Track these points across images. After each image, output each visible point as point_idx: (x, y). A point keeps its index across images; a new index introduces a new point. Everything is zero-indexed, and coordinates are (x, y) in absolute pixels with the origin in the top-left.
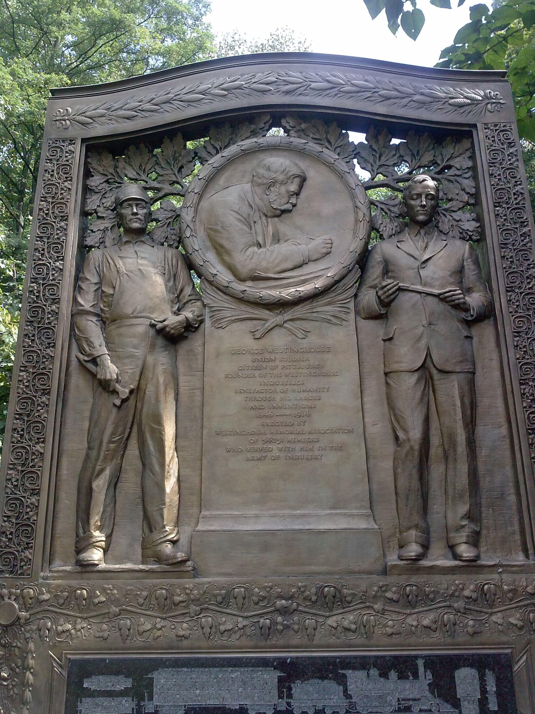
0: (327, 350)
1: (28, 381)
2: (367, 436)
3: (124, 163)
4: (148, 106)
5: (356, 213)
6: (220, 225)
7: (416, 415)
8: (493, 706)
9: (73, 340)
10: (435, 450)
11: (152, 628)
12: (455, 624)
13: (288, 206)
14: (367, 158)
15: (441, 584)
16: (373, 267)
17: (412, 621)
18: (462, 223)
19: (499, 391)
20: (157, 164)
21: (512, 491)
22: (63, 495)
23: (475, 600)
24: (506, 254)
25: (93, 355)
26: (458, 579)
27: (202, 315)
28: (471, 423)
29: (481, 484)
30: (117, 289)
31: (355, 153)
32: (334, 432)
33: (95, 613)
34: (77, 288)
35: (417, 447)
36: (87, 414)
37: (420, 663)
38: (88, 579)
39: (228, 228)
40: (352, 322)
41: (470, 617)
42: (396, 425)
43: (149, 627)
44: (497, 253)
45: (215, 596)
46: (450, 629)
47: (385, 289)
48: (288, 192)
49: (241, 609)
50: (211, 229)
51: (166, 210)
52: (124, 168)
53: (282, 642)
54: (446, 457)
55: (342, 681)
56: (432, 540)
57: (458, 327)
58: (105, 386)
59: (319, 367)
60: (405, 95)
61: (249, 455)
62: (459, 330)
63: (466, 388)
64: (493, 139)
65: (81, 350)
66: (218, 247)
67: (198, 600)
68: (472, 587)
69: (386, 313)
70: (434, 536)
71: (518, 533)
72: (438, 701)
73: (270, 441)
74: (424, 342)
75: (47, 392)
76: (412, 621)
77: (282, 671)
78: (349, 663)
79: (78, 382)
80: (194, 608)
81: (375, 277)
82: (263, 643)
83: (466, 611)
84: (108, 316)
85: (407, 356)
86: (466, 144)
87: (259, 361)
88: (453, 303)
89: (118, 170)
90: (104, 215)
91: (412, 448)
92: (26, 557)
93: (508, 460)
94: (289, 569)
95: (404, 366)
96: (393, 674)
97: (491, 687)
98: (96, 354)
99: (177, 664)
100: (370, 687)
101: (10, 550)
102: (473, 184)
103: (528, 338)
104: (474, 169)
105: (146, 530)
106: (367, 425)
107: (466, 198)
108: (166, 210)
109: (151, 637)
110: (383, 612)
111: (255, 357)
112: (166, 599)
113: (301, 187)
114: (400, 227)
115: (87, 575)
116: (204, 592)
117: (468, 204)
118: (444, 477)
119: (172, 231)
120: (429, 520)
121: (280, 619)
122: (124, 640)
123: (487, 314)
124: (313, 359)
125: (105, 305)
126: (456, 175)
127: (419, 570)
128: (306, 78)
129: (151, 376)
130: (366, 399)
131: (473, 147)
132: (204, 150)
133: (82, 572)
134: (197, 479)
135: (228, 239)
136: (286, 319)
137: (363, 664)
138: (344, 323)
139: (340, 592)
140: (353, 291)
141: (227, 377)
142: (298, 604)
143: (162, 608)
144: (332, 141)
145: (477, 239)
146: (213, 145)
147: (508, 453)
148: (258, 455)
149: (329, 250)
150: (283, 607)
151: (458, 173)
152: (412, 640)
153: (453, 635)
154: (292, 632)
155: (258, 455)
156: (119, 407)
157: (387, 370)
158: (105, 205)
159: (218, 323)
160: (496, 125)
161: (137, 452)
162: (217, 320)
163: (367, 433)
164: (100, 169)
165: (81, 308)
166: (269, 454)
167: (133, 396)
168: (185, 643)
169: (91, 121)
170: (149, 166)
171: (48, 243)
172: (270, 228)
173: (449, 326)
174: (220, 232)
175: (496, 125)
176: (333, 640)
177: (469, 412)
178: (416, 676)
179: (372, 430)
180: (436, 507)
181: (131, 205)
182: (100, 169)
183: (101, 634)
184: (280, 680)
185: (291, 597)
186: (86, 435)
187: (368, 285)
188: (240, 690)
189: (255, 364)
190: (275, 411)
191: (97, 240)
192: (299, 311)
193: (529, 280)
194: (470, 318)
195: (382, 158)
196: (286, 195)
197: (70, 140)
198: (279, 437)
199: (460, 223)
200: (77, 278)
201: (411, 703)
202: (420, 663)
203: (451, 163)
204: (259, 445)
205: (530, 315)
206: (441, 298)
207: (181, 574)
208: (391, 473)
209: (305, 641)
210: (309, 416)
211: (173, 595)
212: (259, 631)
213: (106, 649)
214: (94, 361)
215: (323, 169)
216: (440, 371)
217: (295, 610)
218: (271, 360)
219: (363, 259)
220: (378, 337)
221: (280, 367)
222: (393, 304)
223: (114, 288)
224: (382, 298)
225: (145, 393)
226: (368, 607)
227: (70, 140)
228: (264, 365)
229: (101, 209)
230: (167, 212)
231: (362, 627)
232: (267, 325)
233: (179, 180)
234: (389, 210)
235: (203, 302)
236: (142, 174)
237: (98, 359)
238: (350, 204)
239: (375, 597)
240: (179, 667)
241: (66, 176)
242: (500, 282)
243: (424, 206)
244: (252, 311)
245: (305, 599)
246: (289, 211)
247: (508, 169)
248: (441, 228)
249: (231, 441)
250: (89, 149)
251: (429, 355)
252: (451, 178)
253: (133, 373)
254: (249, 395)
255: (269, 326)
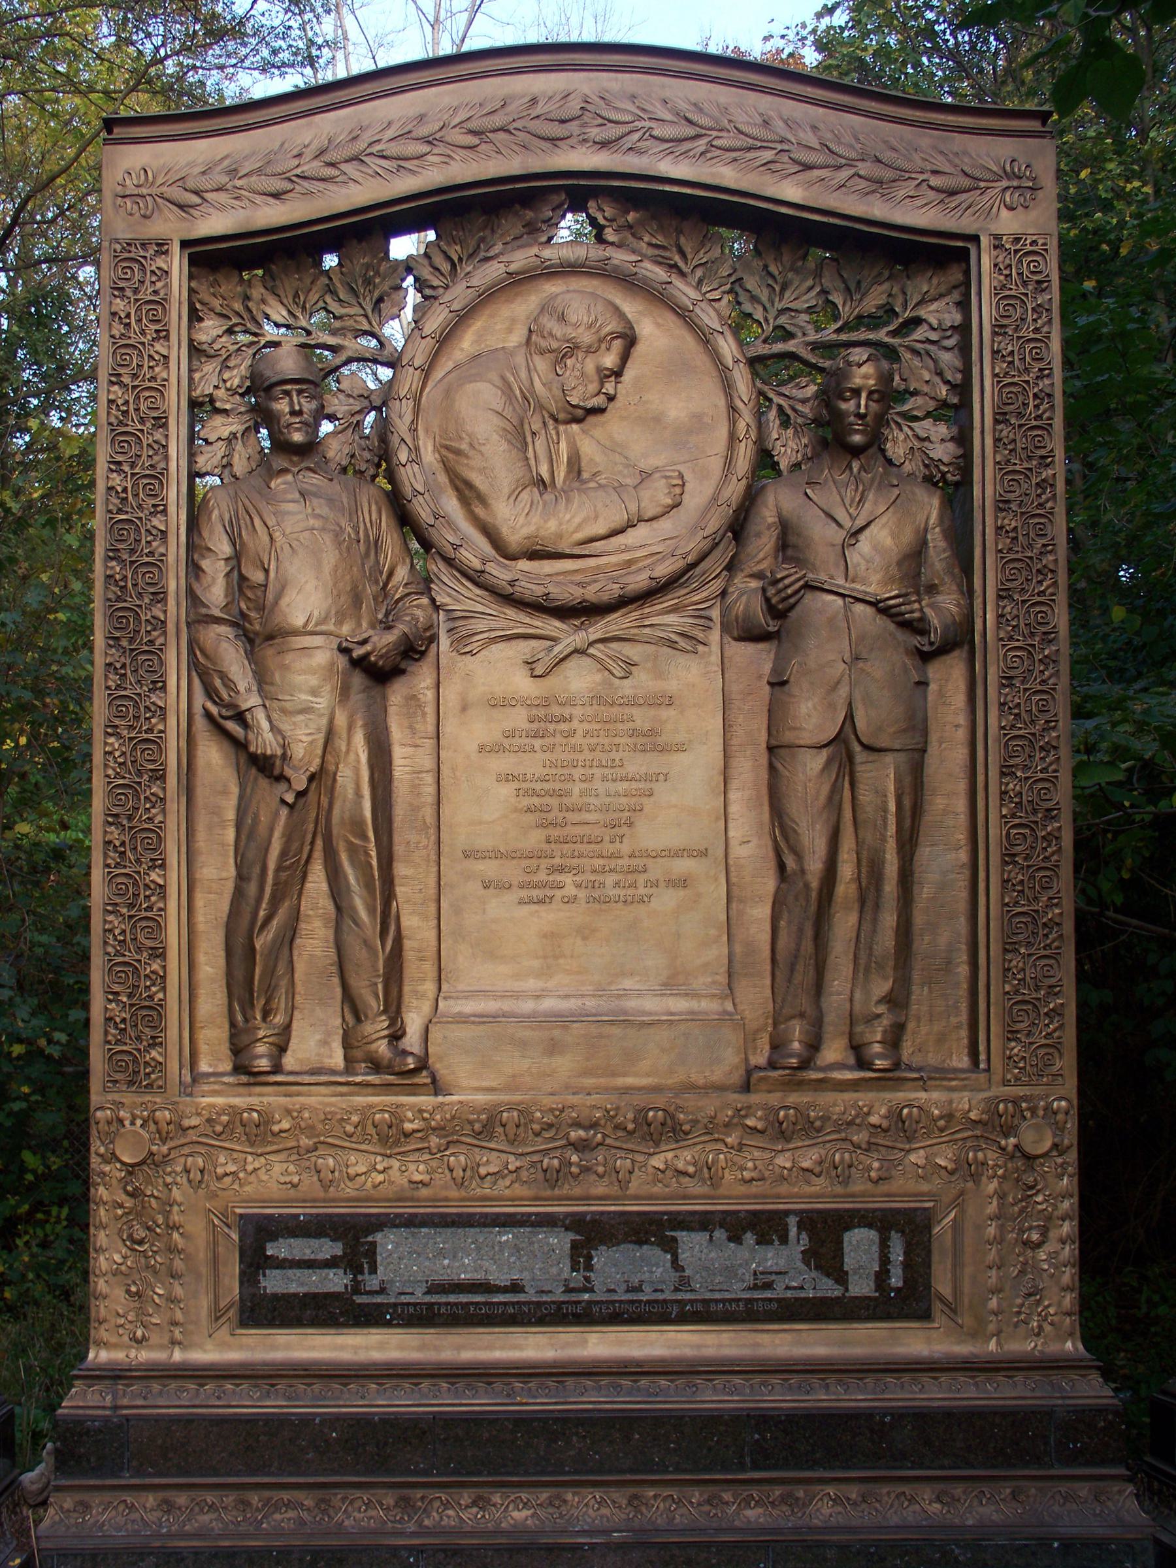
0: (669, 701)
1: (124, 753)
2: (731, 862)
3: (263, 290)
4: (311, 167)
5: (732, 423)
6: (467, 440)
7: (818, 827)
8: (896, 1281)
9: (194, 673)
10: (845, 888)
11: (371, 1177)
12: (850, 1166)
13: (599, 401)
14: (756, 291)
15: (835, 1105)
16: (758, 535)
17: (784, 1161)
18: (931, 446)
19: (962, 786)
20: (332, 292)
21: (965, 958)
22: (201, 958)
23: (886, 1131)
24: (1006, 521)
25: (237, 706)
26: (863, 1098)
27: (431, 626)
28: (908, 843)
29: (915, 946)
30: (272, 574)
31: (732, 279)
32: (678, 853)
33: (275, 1147)
34: (194, 569)
35: (815, 885)
36: (231, 815)
37: (792, 1221)
38: (260, 1095)
39: (483, 449)
40: (715, 648)
41: (875, 1155)
42: (782, 844)
43: (362, 1169)
44: (989, 521)
45: (471, 1122)
46: (841, 1174)
47: (781, 585)
48: (599, 369)
49: (512, 1142)
50: (447, 448)
51: (349, 396)
52: (263, 301)
53: (577, 1191)
54: (862, 901)
55: (671, 1246)
56: (826, 1036)
57: (905, 664)
58: (263, 766)
59: (653, 733)
60: (843, 161)
61: (524, 893)
62: (906, 670)
63: (908, 780)
64: (1007, 272)
65: (211, 693)
66: (461, 486)
67: (443, 1128)
68: (883, 1111)
69: (778, 631)
70: (828, 1029)
71: (965, 1027)
72: (814, 1274)
73: (561, 870)
74: (843, 691)
75: (159, 776)
76: (784, 1161)
77: (577, 1233)
78: (683, 1221)
79: (213, 757)
80: (434, 1141)
81: (761, 555)
82: (549, 1193)
83: (870, 1147)
84: (257, 627)
85: (813, 718)
86: (955, 275)
87: (540, 720)
88: (900, 618)
89: (250, 304)
90: (228, 407)
91: (807, 886)
92: (153, 1059)
93: (962, 906)
94: (589, 1082)
95: (806, 738)
96: (749, 1238)
97: (897, 1254)
98: (244, 706)
99: (411, 1222)
100: (713, 1255)
101: (125, 1048)
102: (958, 363)
103: (1026, 690)
104: (964, 329)
105: (349, 1017)
106: (732, 842)
107: (943, 391)
108: (349, 396)
109: (369, 1184)
110: (740, 1147)
111: (535, 712)
112: (390, 1127)
113: (625, 357)
114: (814, 448)
115: (258, 1089)
116: (453, 1118)
117: (944, 404)
118: (854, 935)
119: (362, 442)
120: (824, 1005)
121: (574, 1158)
122: (326, 1188)
123: (960, 638)
124: (642, 718)
125: (251, 605)
126: (928, 341)
127: (800, 1085)
128: (644, 110)
129: (344, 748)
130: (732, 796)
131: (967, 284)
132: (426, 262)
133: (248, 1084)
134: (433, 934)
135: (482, 470)
136: (592, 638)
137: (703, 1222)
138: (701, 648)
139: (673, 1117)
140: (716, 586)
141: (482, 748)
142: (605, 1136)
143: (384, 1140)
144: (688, 250)
145: (954, 488)
146: (444, 252)
147: (964, 895)
148: (536, 893)
149: (678, 499)
150: (575, 1138)
151: (934, 336)
152: (783, 1189)
153: (846, 1181)
154: (595, 1177)
155: (536, 893)
156: (291, 807)
157: (774, 743)
158: (228, 385)
159: (461, 643)
160: (1017, 240)
161: (324, 886)
162: (463, 637)
163: (732, 856)
164: (216, 303)
165: (204, 611)
166: (559, 894)
167: (314, 785)
168: (424, 1192)
169: (197, 200)
170: (314, 297)
171: (133, 475)
172: (563, 446)
173: (888, 662)
174: (467, 457)
175: (1017, 240)
176: (657, 1189)
177: (908, 823)
178: (784, 1240)
179: (739, 852)
180: (839, 983)
181: (287, 393)
182: (216, 303)
183: (288, 1179)
184: (574, 1246)
185: (594, 1125)
186: (232, 853)
187: (748, 571)
188: (512, 1259)
189: (535, 726)
190: (569, 815)
191: (216, 461)
192: (615, 623)
193: (1040, 577)
194: (925, 649)
195: (787, 294)
196: (596, 378)
197: (158, 245)
198: (575, 862)
199: (926, 444)
200: (191, 547)
201: (773, 1277)
202: (792, 1221)
203: (922, 313)
204: (542, 876)
205: (1033, 646)
206: (880, 607)
207: (414, 1089)
208: (767, 927)
209: (615, 1190)
210: (631, 825)
211: (402, 1121)
212: (540, 1175)
213: (297, 1201)
214: (240, 717)
215: (670, 319)
216: (867, 748)
217: (599, 1144)
218: (562, 719)
219: (738, 527)
220: (760, 677)
221: (580, 733)
222: (793, 615)
223: (267, 571)
224: (774, 601)
225: (335, 780)
226: (716, 1140)
227: (158, 245)
228: (551, 727)
229: (221, 393)
230: (351, 401)
231: (705, 1170)
232: (557, 649)
233: (376, 329)
234: (795, 410)
235: (433, 600)
236: (299, 314)
237: (248, 716)
238: (722, 403)
239: (727, 1125)
240: (415, 1226)
241: (157, 327)
242: (989, 575)
243: (860, 416)
244: (527, 620)
245: (617, 1127)
246: (601, 411)
247: (1029, 341)
248: (889, 453)
249: (489, 868)
250: (194, 261)
251: (850, 717)
252: (919, 346)
253: (311, 742)
254: (524, 785)
255: (560, 652)
